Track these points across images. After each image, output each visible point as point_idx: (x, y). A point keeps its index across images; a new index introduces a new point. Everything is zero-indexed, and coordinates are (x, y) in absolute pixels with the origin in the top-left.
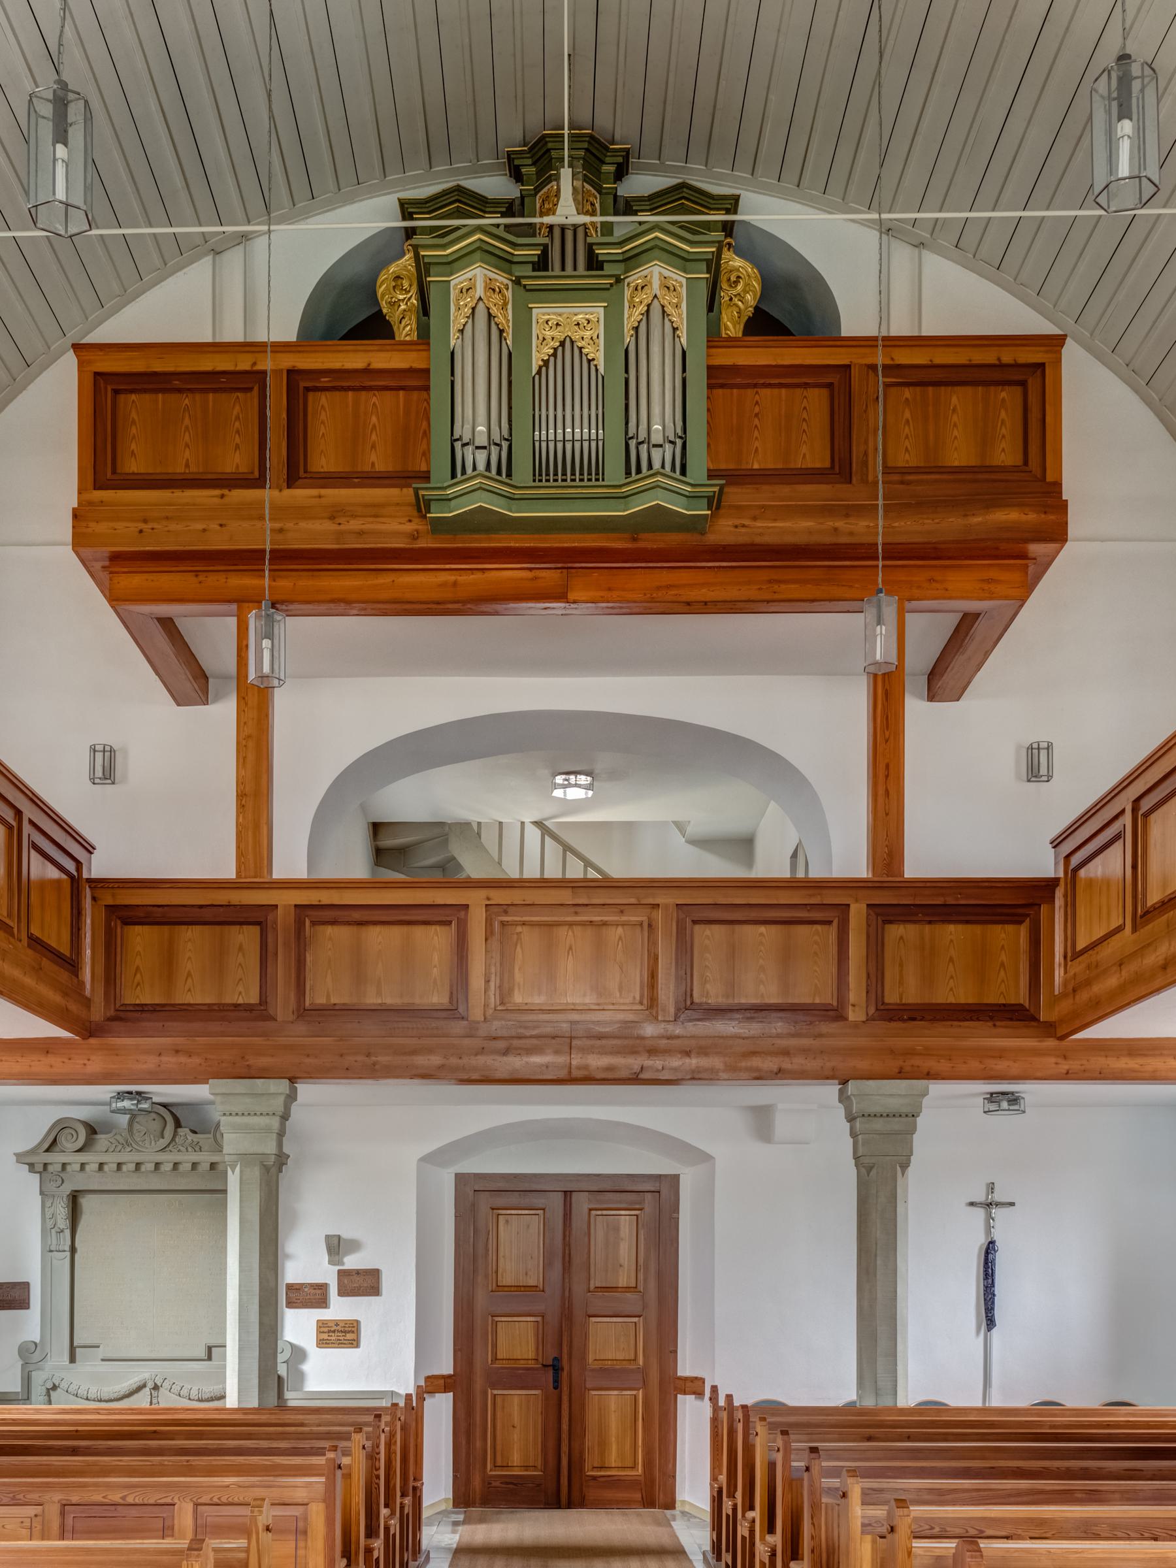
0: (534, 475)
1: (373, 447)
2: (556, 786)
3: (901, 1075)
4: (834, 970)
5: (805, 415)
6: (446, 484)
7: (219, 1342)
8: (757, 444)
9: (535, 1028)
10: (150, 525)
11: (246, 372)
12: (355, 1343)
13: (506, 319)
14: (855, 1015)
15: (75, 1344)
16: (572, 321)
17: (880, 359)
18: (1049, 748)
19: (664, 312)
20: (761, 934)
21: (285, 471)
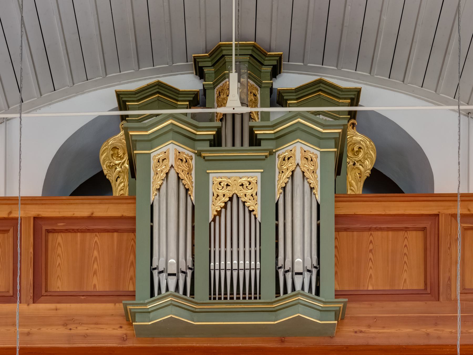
0: (210, 294)
1: (95, 273)
5: (405, 251)
6: (146, 301)
8: (371, 272)
11: (4, 219)
13: (190, 181)
16: (236, 182)
17: (459, 210)
19: (304, 176)
21: (32, 291)
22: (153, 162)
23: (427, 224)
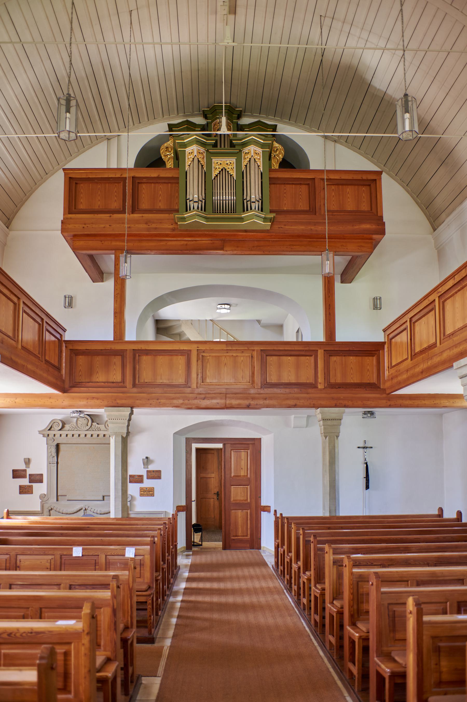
1: (160, 201)
2: (218, 309)
3: (336, 406)
4: (314, 372)
5: (300, 193)
7: (107, 494)
9: (214, 390)
10: (86, 226)
12: (153, 495)
14: (320, 386)
15: (58, 495)
16: (224, 163)
18: (380, 298)
20: (289, 360)
22: (187, 154)
23: (310, 182)
